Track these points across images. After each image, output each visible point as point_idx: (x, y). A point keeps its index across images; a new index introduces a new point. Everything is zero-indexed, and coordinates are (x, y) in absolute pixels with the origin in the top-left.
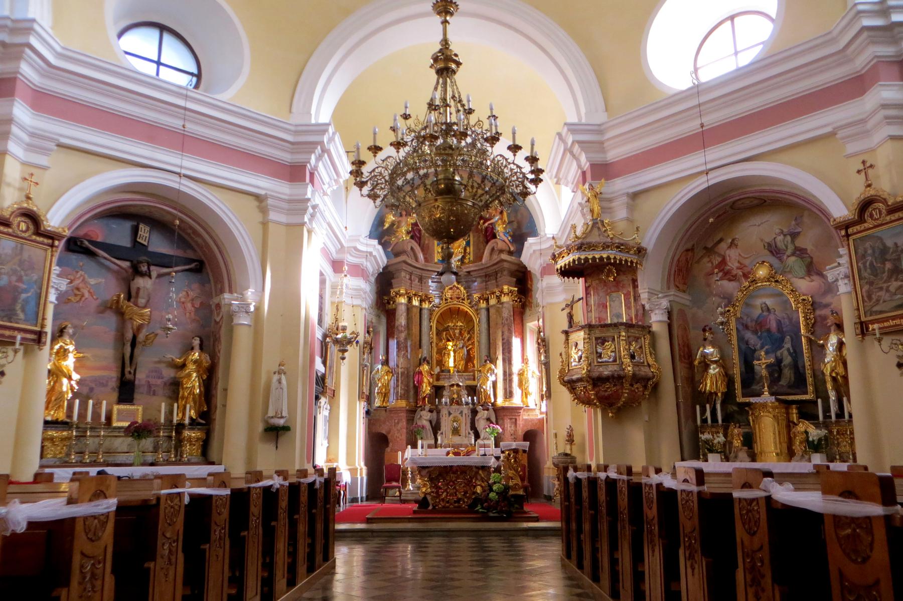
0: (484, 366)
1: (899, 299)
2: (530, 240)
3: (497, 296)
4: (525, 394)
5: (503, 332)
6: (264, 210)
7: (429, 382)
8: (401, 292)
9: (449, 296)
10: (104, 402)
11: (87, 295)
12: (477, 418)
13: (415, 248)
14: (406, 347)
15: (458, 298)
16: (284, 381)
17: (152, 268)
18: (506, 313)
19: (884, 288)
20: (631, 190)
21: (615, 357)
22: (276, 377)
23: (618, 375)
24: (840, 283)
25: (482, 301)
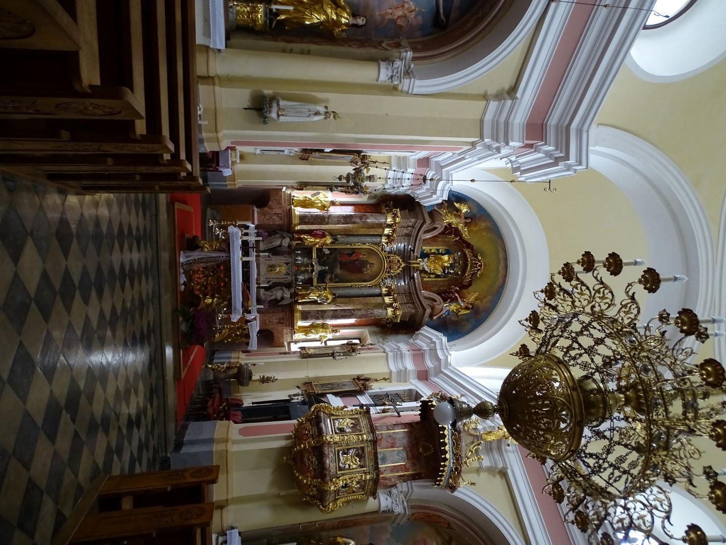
3: (392, 304)
4: (306, 330)
5: (360, 310)
6: (499, 96)
8: (397, 219)
9: (391, 260)
12: (284, 288)
13: (436, 230)
16: (316, 118)
18: (378, 312)
20: (509, 471)
21: (344, 469)
22: (322, 109)
23: (326, 474)
25: (387, 289)
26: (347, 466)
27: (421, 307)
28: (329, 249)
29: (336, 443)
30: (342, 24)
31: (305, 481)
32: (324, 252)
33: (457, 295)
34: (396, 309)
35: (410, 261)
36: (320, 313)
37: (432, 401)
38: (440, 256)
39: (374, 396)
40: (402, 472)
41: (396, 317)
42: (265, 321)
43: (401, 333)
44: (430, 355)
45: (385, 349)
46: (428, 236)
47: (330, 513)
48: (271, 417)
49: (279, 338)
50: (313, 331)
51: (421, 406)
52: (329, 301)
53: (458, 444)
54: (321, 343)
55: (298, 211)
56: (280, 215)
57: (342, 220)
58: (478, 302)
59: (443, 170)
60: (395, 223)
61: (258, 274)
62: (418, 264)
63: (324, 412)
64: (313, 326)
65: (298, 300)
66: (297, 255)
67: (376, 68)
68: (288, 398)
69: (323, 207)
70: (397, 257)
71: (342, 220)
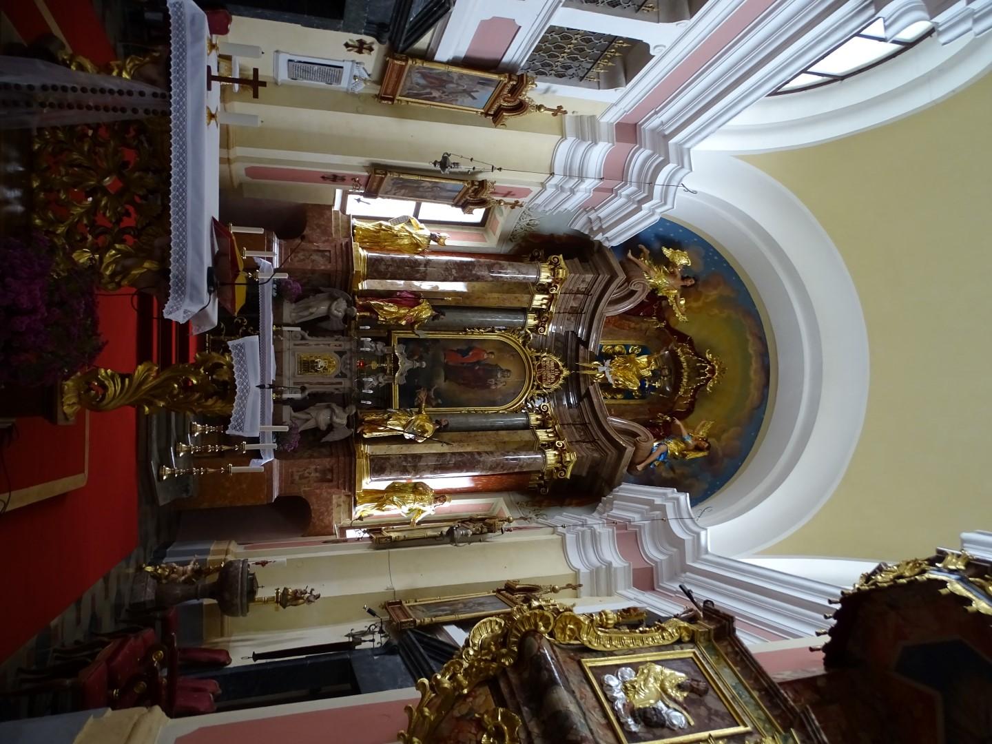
0: (430, 420)
2: (684, 498)
4: (380, 498)
7: (399, 319)
9: (543, 363)
12: (334, 406)
15: (540, 379)
34: (562, 452)
36: (410, 459)
42: (292, 476)
43: (570, 505)
48: (304, 692)
49: (322, 514)
56: (327, 254)
59: (671, 142)
64: (392, 489)
70: (554, 358)
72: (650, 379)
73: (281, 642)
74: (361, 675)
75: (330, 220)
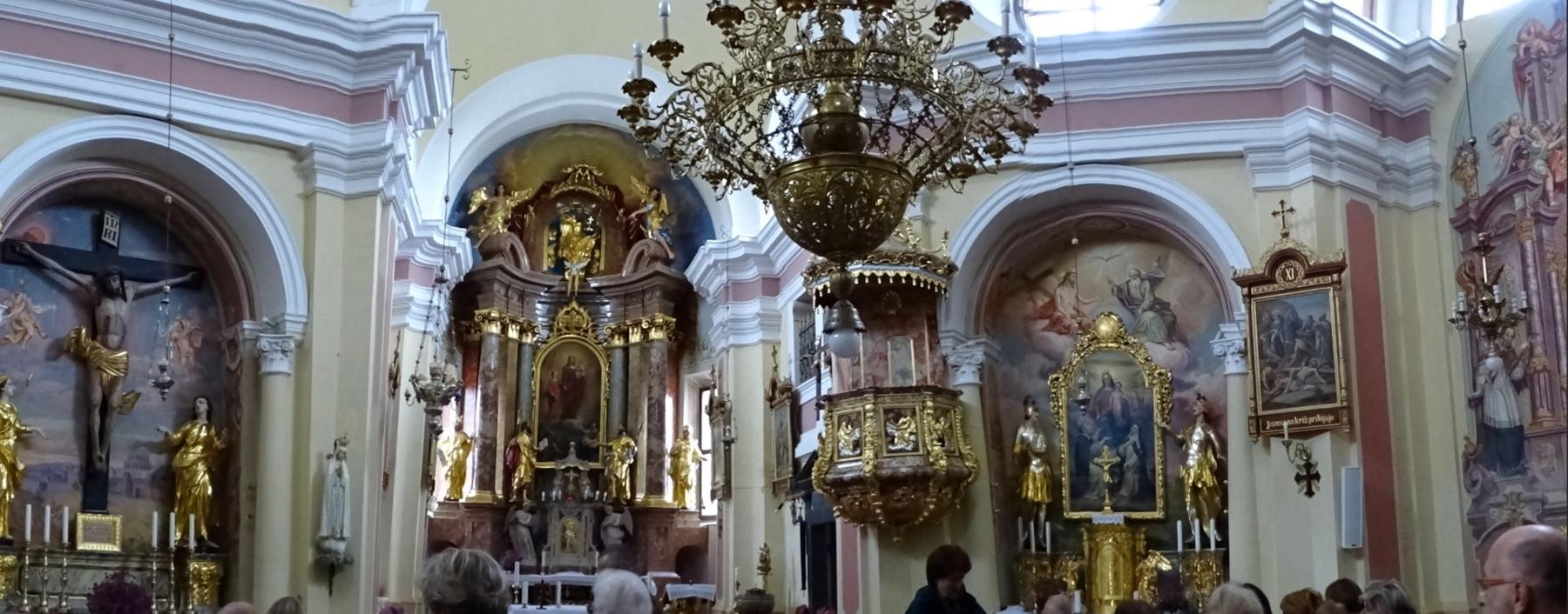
1: (1308, 390)
3: (642, 329)
4: (681, 486)
5: (650, 387)
6: (307, 174)
8: (493, 315)
10: (66, 509)
11: (31, 331)
12: (605, 524)
13: (516, 247)
14: (496, 404)
16: (346, 475)
17: (127, 283)
18: (656, 356)
19: (1291, 373)
21: (916, 443)
22: (333, 465)
24: (1229, 358)
26: (912, 438)
27: (652, 279)
28: (540, 439)
29: (876, 456)
30: (208, 436)
31: (932, 507)
32: (546, 448)
33: (633, 215)
34: (652, 324)
35: (569, 292)
37: (817, 291)
38: (562, 239)
39: (802, 374)
40: (924, 345)
41: (667, 323)
44: (735, 271)
45: (723, 349)
46: (525, 261)
47: (979, 466)
48: (829, 556)
50: (683, 474)
51: (823, 307)
52: (633, 443)
53: (887, 256)
54: (705, 460)
55: (469, 491)
57: (490, 413)
58: (648, 178)
59: (415, 234)
60: (501, 319)
61: (576, 569)
62: (574, 278)
63: (827, 473)
64: (675, 474)
65: (626, 500)
66: (548, 498)
67: (271, 378)
68: (798, 526)
69: (465, 445)
71: (490, 413)
72: (584, 226)
73: (794, 577)
74: (823, 519)
75: (442, 520)
